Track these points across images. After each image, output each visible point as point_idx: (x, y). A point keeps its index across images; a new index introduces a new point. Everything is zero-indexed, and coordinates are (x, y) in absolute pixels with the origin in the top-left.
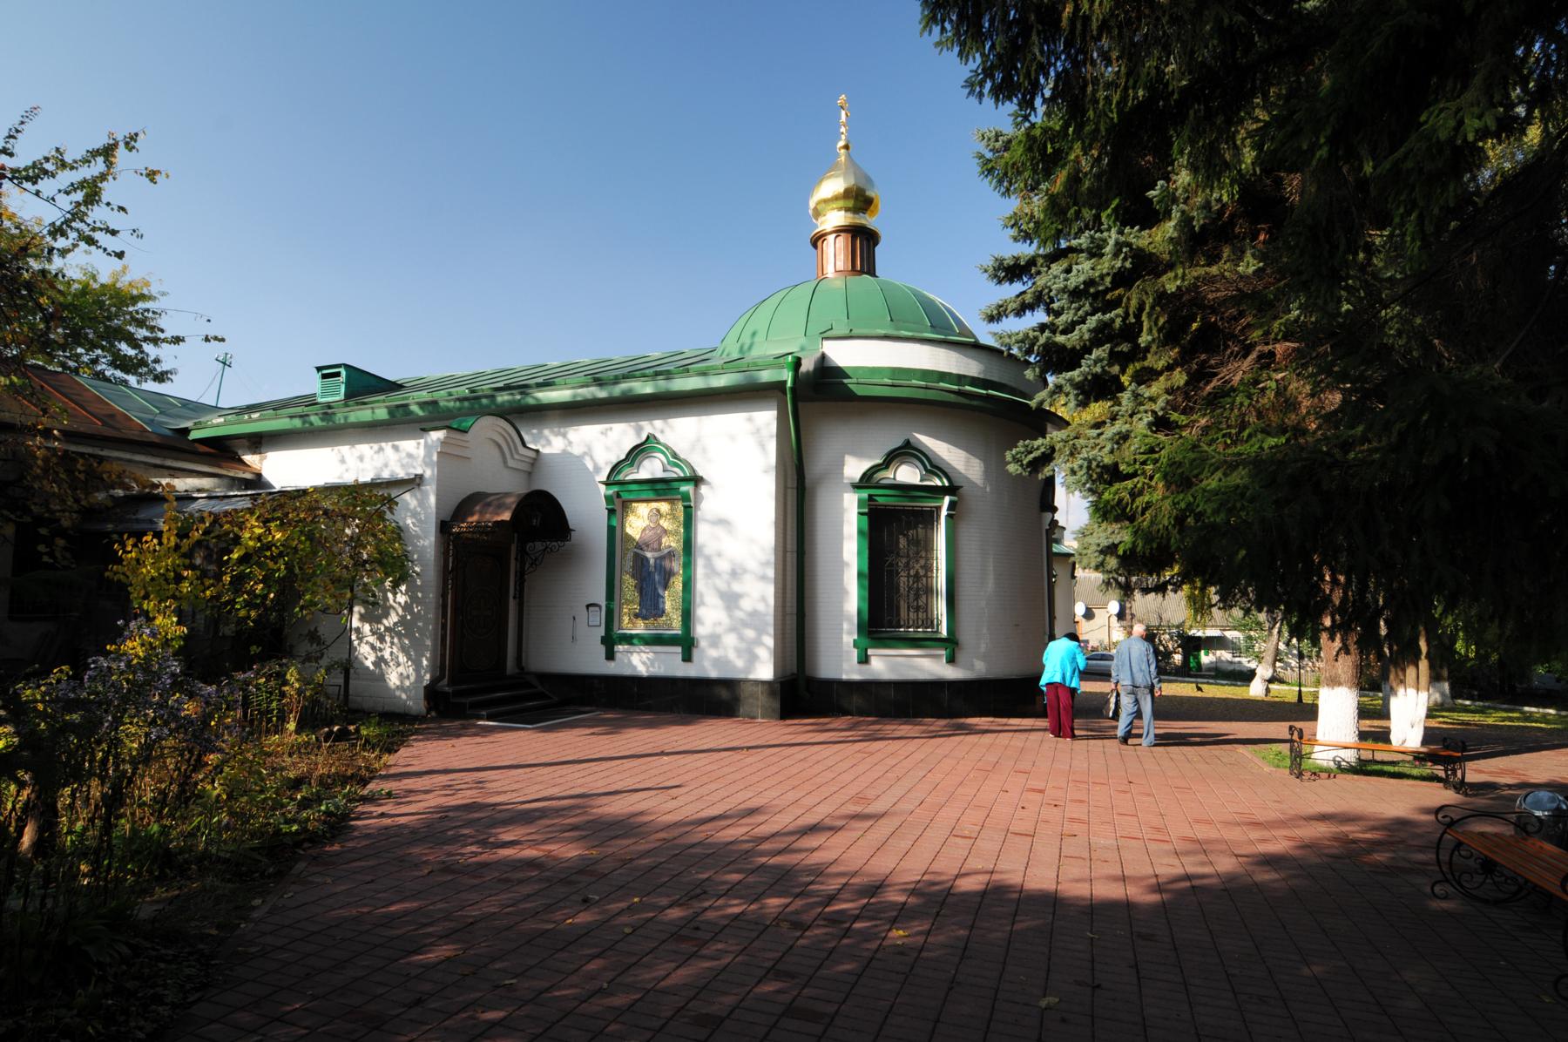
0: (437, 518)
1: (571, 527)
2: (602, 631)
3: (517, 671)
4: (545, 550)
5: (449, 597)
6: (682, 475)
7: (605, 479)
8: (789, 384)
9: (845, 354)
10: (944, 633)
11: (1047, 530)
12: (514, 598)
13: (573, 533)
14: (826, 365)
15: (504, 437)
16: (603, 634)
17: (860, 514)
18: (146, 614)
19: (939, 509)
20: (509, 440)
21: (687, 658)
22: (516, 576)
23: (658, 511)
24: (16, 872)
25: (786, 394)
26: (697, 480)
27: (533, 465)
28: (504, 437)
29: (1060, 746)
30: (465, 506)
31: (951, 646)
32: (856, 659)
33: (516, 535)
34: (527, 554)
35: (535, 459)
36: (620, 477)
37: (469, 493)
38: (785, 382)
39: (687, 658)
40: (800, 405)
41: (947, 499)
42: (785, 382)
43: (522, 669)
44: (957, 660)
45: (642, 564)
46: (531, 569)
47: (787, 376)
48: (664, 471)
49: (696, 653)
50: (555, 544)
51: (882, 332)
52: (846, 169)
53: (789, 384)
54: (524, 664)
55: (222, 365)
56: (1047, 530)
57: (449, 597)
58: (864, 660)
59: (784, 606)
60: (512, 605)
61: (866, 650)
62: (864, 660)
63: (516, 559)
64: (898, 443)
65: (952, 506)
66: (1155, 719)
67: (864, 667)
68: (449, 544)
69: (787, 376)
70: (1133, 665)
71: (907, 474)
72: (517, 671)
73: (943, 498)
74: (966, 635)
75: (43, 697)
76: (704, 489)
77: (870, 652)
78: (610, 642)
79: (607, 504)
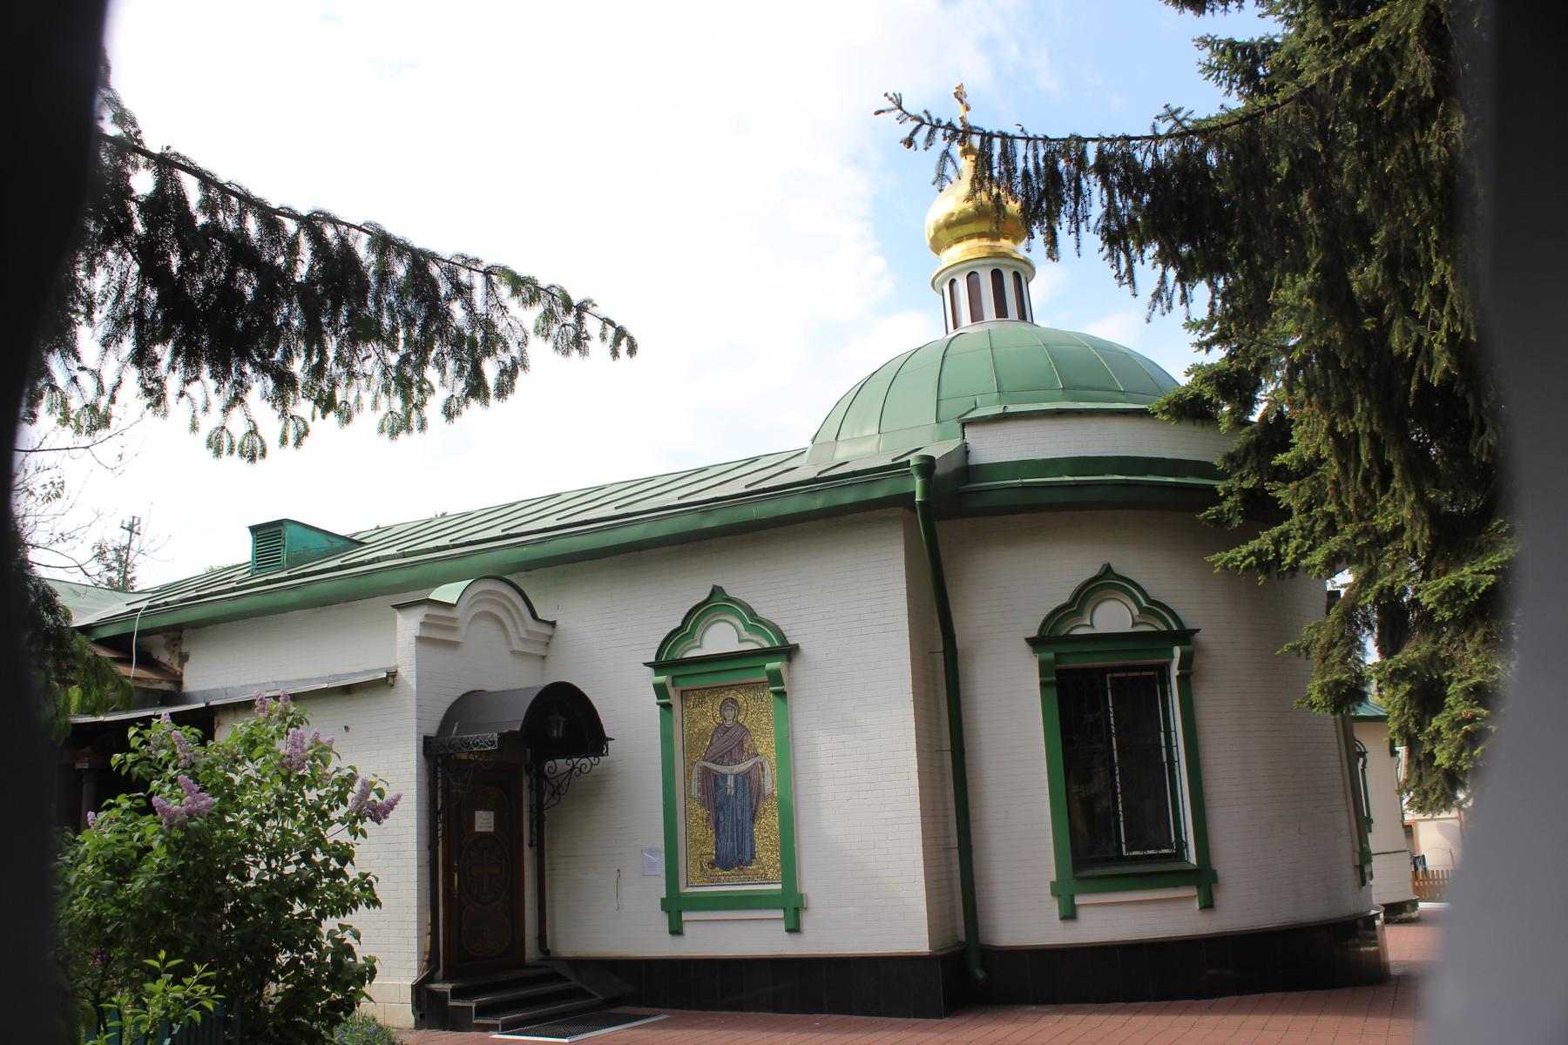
0: (418, 733)
1: (608, 734)
3: (541, 956)
5: (440, 847)
6: (767, 645)
12: (531, 845)
13: (610, 743)
14: (973, 461)
17: (1043, 685)
18: (191, 849)
19: (1163, 670)
20: (506, 602)
21: (794, 929)
22: (531, 811)
23: (379, 813)
26: (788, 652)
29: (1368, 1021)
30: (464, 709)
31: (1204, 880)
32: (1058, 917)
33: (528, 750)
34: (546, 778)
36: (678, 655)
39: (794, 929)
40: (940, 527)
43: (548, 952)
44: (1217, 903)
46: (553, 802)
48: (740, 641)
49: (807, 921)
50: (585, 760)
54: (549, 947)
55: (128, 532)
57: (440, 847)
58: (1069, 914)
60: (528, 854)
61: (1072, 898)
62: (1069, 914)
63: (530, 787)
64: (1092, 571)
65: (1186, 661)
67: (1070, 925)
68: (436, 772)
71: (1113, 617)
72: (541, 956)
75: (1421, 438)
76: (798, 665)
77: (1078, 900)
78: (675, 907)
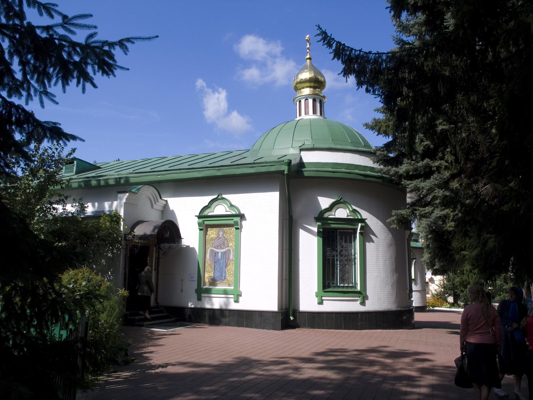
2: (196, 287)
4: (169, 247)
7: (198, 215)
8: (286, 172)
9: (309, 157)
10: (359, 288)
11: (407, 239)
13: (183, 240)
15: (153, 196)
16: (317, 291)
24: (513, 275)
25: (284, 176)
27: (164, 207)
28: (153, 196)
35: (165, 205)
37: (136, 221)
38: (284, 171)
41: (360, 225)
42: (284, 171)
43: (158, 304)
45: (215, 255)
46: (163, 257)
47: (285, 168)
51: (326, 146)
52: (310, 69)
53: (286, 172)
56: (407, 239)
58: (321, 303)
59: (282, 276)
63: (156, 251)
66: (309, 114)
69: (285, 168)
70: (282, 158)
72: (156, 304)
73: (358, 224)
74: (370, 292)
79: (199, 226)
